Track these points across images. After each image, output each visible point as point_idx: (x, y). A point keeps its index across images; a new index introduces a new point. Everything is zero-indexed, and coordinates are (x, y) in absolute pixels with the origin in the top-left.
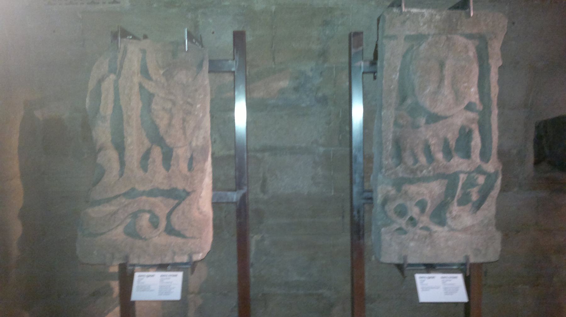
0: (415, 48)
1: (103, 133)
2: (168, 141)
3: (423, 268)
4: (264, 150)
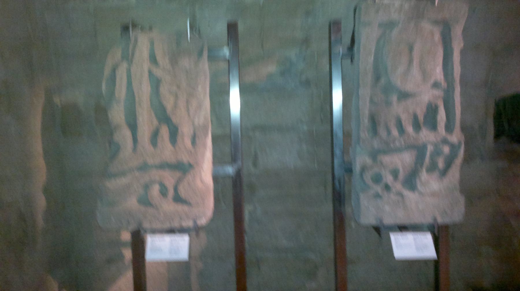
1: (117, 114)
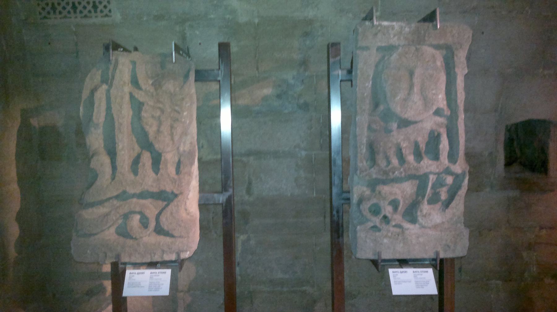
0: (386, 58)
1: (96, 140)
2: (157, 146)
3: (397, 263)
4: (249, 153)
